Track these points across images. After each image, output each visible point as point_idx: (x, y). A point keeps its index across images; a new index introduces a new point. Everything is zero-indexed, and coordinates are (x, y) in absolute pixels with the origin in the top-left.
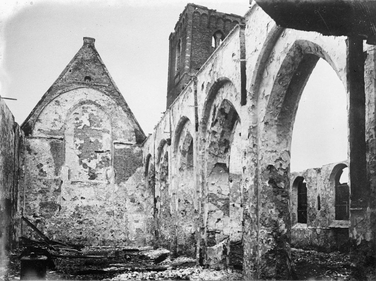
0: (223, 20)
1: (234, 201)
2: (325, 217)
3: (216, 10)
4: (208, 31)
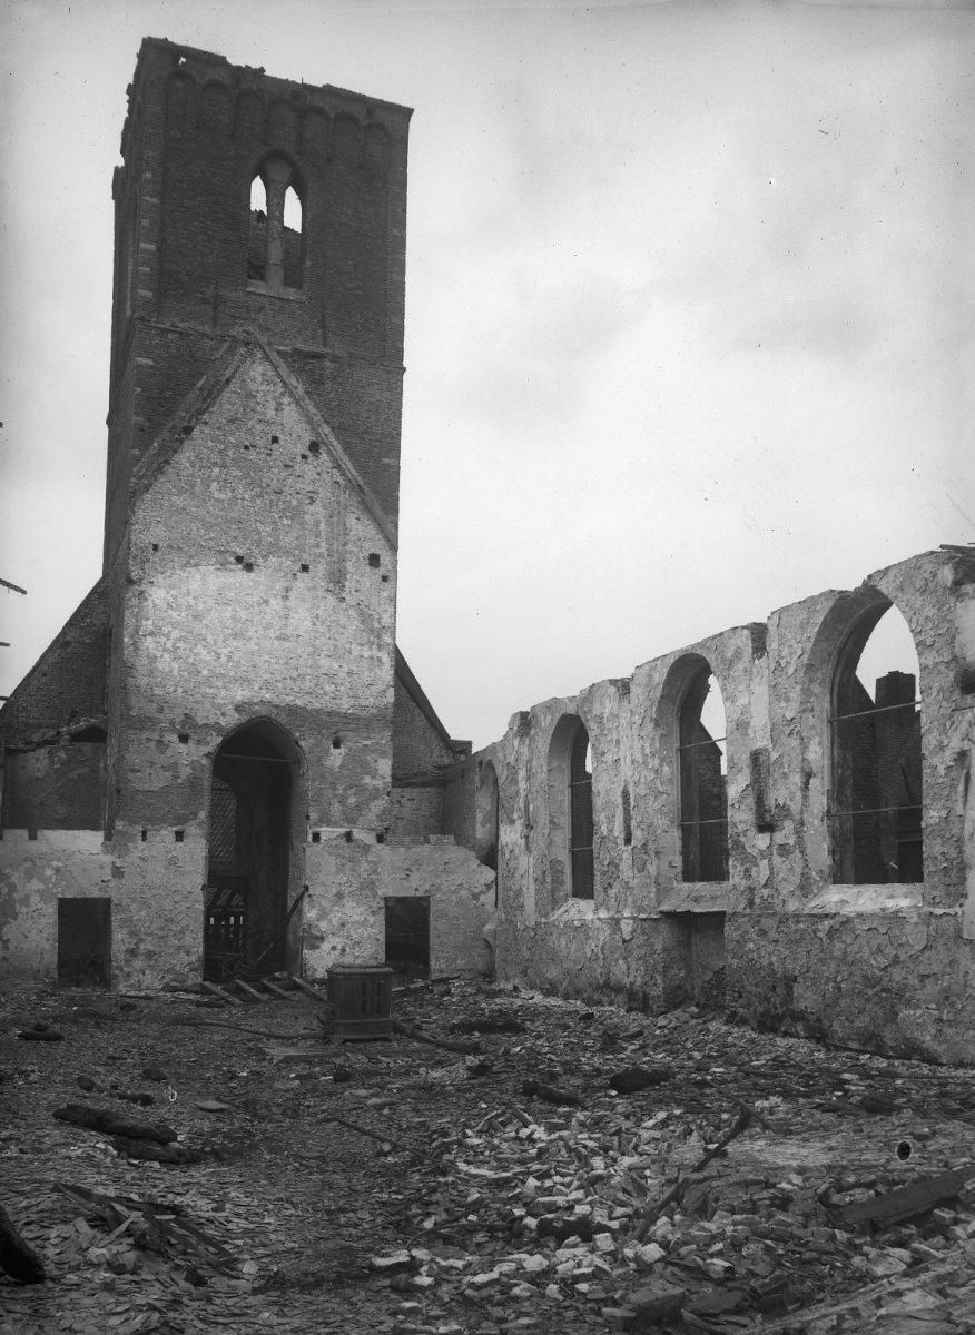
2: (645, 873)
3: (262, 70)
4: (232, 153)
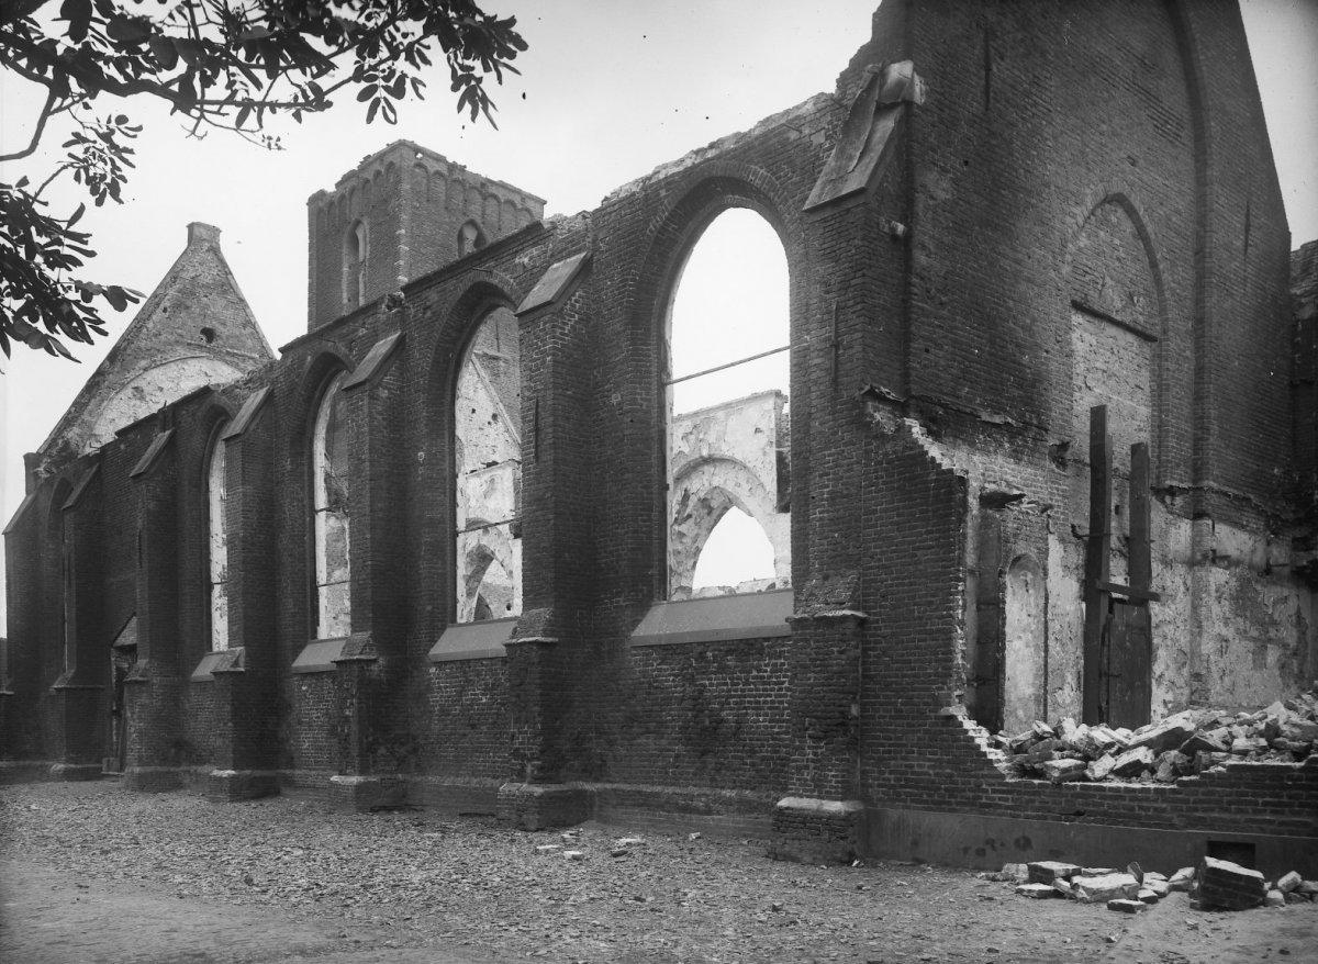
0: (480, 193)
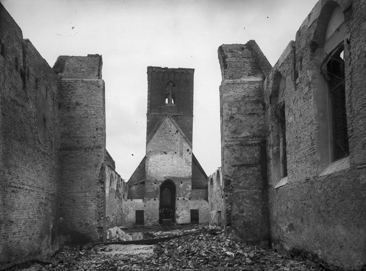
1: (184, 196)
